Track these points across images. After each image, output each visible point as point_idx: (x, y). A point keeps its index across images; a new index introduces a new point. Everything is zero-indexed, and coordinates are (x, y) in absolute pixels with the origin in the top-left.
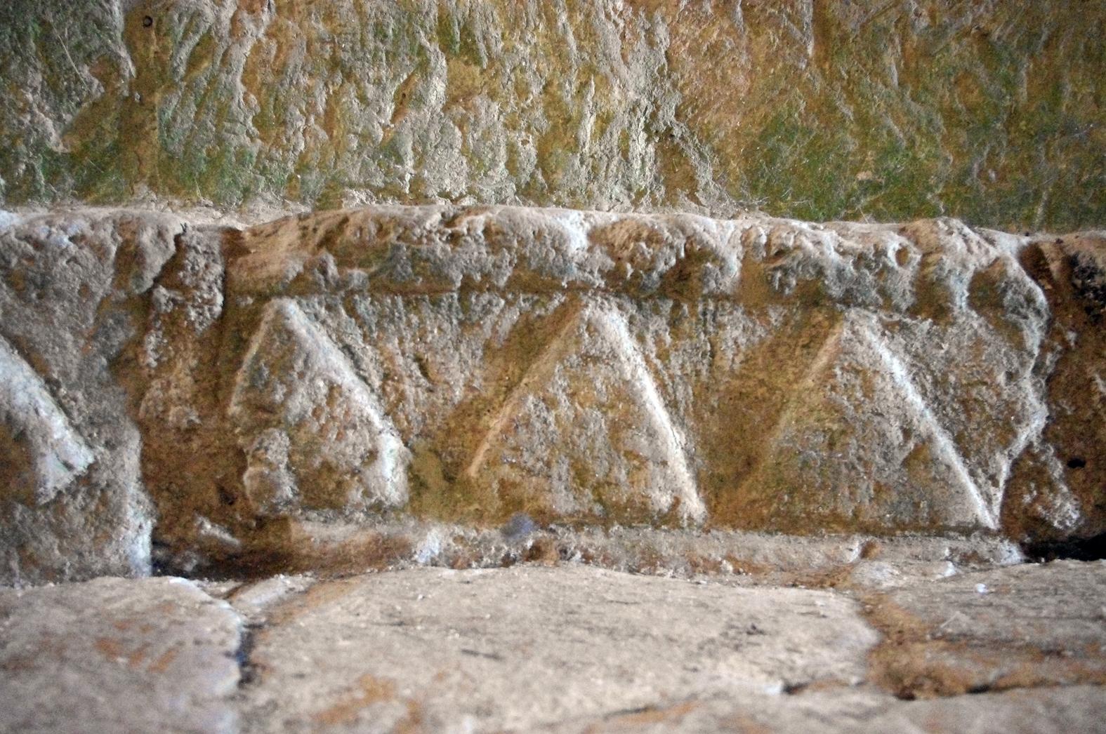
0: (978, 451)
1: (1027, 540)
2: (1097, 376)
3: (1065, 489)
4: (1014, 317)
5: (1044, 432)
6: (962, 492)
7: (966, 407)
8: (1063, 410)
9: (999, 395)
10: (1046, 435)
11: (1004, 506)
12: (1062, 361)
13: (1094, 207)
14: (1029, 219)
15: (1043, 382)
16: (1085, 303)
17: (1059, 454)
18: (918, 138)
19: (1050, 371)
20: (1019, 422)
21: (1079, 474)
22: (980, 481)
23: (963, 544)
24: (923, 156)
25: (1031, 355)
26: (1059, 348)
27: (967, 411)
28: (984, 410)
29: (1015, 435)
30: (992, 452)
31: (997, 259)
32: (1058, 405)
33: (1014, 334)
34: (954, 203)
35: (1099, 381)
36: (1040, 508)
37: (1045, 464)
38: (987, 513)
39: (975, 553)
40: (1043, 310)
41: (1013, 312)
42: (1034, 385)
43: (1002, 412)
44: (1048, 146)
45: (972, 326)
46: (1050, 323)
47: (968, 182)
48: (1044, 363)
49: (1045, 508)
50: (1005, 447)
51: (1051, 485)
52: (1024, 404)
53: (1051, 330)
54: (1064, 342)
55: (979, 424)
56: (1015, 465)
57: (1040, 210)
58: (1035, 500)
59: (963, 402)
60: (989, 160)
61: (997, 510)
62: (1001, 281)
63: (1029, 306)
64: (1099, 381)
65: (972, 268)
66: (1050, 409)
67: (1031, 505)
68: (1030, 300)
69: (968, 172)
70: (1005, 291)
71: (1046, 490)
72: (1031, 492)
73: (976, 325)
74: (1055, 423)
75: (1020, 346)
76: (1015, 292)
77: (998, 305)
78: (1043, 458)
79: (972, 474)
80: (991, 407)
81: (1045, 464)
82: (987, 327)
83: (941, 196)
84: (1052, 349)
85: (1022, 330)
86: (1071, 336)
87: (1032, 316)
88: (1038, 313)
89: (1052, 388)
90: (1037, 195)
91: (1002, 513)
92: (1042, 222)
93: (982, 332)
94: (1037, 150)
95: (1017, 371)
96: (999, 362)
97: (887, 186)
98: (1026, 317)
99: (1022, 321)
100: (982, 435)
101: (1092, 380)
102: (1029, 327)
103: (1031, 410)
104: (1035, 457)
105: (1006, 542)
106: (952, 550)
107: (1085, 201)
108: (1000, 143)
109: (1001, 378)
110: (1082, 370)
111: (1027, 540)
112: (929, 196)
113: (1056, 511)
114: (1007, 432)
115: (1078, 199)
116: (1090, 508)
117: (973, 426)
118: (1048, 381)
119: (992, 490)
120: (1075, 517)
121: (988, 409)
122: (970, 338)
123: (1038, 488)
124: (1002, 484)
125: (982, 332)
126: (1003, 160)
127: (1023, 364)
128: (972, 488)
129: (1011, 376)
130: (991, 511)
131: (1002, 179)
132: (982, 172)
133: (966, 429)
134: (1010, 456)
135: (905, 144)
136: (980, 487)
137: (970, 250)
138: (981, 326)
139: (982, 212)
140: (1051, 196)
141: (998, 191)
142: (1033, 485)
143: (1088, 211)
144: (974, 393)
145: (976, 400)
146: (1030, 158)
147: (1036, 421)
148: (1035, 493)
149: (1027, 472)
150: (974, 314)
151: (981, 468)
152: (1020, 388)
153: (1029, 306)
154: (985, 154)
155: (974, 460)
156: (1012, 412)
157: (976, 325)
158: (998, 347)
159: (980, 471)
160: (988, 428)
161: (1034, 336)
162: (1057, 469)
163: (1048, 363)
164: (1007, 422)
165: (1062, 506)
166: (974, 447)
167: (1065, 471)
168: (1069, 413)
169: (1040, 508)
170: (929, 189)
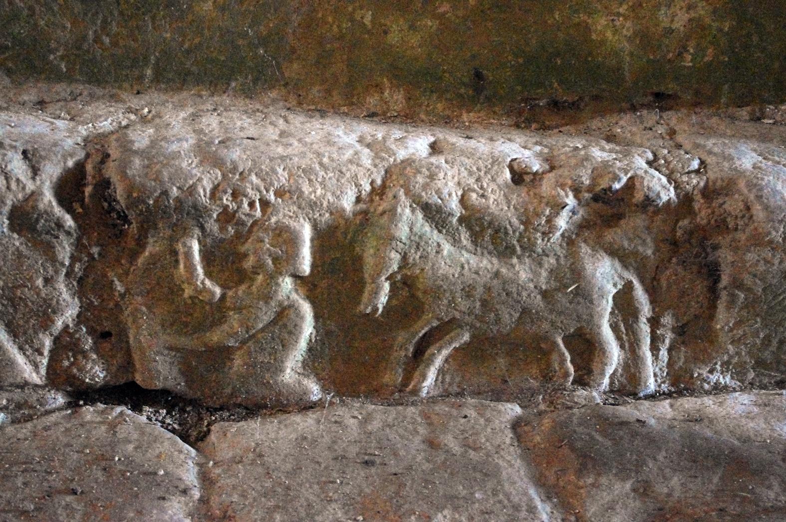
0: (25, 333)
1: (69, 389)
2: (115, 279)
3: (95, 356)
4: (48, 237)
5: (78, 316)
6: (12, 363)
7: (13, 302)
8: (92, 302)
9: (38, 294)
10: (80, 319)
11: (49, 367)
12: (87, 270)
13: (194, 69)
14: (141, 78)
15: (75, 283)
16: (110, 222)
17: (91, 331)
18: (37, 8)
19: (79, 275)
20: (54, 312)
21: (107, 346)
22: (27, 353)
23: (17, 395)
24: (42, 23)
25: (63, 264)
26: (86, 259)
27: (14, 306)
28: (26, 305)
29: (53, 322)
30: (36, 333)
31: (33, 193)
32: (87, 298)
33: (48, 251)
34: (75, 64)
35: (117, 282)
36: (75, 371)
37: (79, 339)
38: (34, 375)
39: (26, 402)
40: (72, 231)
41: (46, 234)
42: (67, 286)
43: (41, 306)
44: (153, 18)
45: (14, 245)
46: (79, 239)
47: (85, 46)
48: (74, 271)
49: (78, 370)
50: (45, 330)
51: (85, 354)
52: (58, 302)
53: (79, 246)
54: (91, 256)
55: (24, 314)
56: (57, 340)
57: (149, 72)
58: (72, 364)
59: (11, 300)
60: (103, 28)
61: (43, 371)
62: (33, 213)
63: (59, 230)
64: (117, 282)
65: (9, 203)
66: (81, 302)
67: (68, 367)
68: (59, 225)
69: (84, 38)
70: (37, 220)
71: (80, 357)
72: (68, 359)
73: (17, 244)
74: (87, 310)
75: (53, 259)
76: (46, 221)
77: (32, 229)
78: (77, 336)
79: (21, 348)
80: (33, 303)
81: (79, 339)
82: (26, 244)
83: (62, 58)
84: (80, 261)
85: (54, 247)
86: (95, 250)
87: (62, 236)
88: (68, 233)
89: (82, 288)
90: (146, 59)
91: (47, 373)
92: (152, 81)
93: (23, 248)
94: (144, 21)
95: (52, 277)
96: (38, 271)
97: (13, 47)
98: (57, 237)
99: (54, 240)
100: (27, 322)
101: (113, 281)
102: (61, 244)
103: (64, 304)
104: (71, 335)
105: (53, 392)
106: (8, 400)
107: (188, 64)
108: (111, 13)
109: (40, 282)
110: (105, 275)
111: (69, 389)
112: (52, 57)
113: (87, 372)
114: (46, 323)
115: (182, 63)
116: (114, 369)
117: (19, 315)
118: (78, 282)
119: (38, 358)
120: (102, 375)
121: (30, 304)
122: (13, 254)
123: (74, 356)
124: (46, 353)
125: (23, 248)
126: (115, 28)
127: (57, 272)
128: (20, 359)
129: (47, 281)
130: (38, 373)
131: (115, 44)
132: (97, 40)
133: (14, 318)
134: (51, 335)
135: (26, 12)
136: (28, 357)
137: (8, 188)
138: (21, 244)
139: (99, 72)
140: (158, 60)
141: (113, 55)
142: (70, 354)
143: (189, 73)
144: (19, 293)
145: (20, 298)
146: (137, 27)
147: (69, 313)
148: (72, 359)
149: (65, 344)
150: (16, 236)
151: (27, 343)
152: (55, 289)
153: (59, 230)
154: (99, 22)
155: (22, 339)
156: (50, 306)
157: (17, 244)
158: (38, 260)
159: (27, 346)
160: (31, 317)
161: (65, 251)
162: (88, 343)
163: (76, 270)
164: (45, 313)
165: (92, 368)
166: (21, 330)
167: (95, 343)
168: (96, 303)
169: (75, 371)
170: (51, 51)
